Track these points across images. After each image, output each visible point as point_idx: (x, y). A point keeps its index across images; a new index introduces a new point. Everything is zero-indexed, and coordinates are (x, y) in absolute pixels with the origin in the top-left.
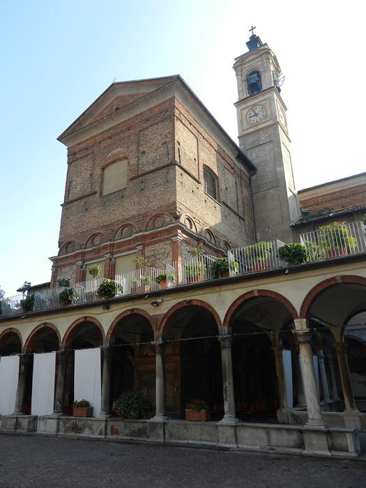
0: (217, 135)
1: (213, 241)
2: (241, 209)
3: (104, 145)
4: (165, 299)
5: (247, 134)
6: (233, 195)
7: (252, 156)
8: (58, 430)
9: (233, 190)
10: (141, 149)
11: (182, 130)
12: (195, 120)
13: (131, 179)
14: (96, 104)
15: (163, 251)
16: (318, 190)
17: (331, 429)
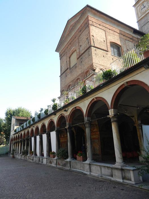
0: (118, 26)
3: (69, 47)
4: (68, 107)
8: (47, 163)
10: (80, 45)
11: (95, 29)
12: (102, 22)
13: (78, 59)
14: (64, 32)
17: (123, 168)
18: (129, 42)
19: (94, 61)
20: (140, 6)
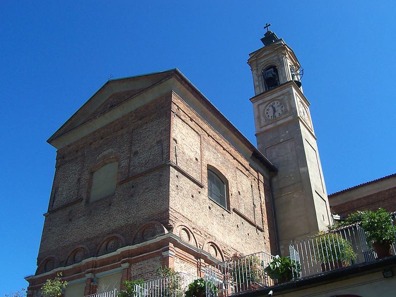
1: (219, 257)
2: (259, 217)
5: (267, 131)
6: (249, 200)
7: (271, 157)
9: (249, 195)
10: (134, 149)
11: (182, 126)
15: (151, 269)
16: (344, 196)
18: (242, 174)
19: (171, 204)
20: (265, 105)
